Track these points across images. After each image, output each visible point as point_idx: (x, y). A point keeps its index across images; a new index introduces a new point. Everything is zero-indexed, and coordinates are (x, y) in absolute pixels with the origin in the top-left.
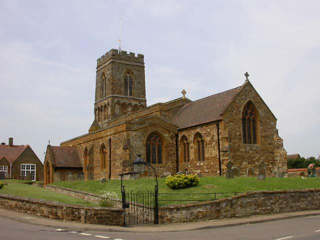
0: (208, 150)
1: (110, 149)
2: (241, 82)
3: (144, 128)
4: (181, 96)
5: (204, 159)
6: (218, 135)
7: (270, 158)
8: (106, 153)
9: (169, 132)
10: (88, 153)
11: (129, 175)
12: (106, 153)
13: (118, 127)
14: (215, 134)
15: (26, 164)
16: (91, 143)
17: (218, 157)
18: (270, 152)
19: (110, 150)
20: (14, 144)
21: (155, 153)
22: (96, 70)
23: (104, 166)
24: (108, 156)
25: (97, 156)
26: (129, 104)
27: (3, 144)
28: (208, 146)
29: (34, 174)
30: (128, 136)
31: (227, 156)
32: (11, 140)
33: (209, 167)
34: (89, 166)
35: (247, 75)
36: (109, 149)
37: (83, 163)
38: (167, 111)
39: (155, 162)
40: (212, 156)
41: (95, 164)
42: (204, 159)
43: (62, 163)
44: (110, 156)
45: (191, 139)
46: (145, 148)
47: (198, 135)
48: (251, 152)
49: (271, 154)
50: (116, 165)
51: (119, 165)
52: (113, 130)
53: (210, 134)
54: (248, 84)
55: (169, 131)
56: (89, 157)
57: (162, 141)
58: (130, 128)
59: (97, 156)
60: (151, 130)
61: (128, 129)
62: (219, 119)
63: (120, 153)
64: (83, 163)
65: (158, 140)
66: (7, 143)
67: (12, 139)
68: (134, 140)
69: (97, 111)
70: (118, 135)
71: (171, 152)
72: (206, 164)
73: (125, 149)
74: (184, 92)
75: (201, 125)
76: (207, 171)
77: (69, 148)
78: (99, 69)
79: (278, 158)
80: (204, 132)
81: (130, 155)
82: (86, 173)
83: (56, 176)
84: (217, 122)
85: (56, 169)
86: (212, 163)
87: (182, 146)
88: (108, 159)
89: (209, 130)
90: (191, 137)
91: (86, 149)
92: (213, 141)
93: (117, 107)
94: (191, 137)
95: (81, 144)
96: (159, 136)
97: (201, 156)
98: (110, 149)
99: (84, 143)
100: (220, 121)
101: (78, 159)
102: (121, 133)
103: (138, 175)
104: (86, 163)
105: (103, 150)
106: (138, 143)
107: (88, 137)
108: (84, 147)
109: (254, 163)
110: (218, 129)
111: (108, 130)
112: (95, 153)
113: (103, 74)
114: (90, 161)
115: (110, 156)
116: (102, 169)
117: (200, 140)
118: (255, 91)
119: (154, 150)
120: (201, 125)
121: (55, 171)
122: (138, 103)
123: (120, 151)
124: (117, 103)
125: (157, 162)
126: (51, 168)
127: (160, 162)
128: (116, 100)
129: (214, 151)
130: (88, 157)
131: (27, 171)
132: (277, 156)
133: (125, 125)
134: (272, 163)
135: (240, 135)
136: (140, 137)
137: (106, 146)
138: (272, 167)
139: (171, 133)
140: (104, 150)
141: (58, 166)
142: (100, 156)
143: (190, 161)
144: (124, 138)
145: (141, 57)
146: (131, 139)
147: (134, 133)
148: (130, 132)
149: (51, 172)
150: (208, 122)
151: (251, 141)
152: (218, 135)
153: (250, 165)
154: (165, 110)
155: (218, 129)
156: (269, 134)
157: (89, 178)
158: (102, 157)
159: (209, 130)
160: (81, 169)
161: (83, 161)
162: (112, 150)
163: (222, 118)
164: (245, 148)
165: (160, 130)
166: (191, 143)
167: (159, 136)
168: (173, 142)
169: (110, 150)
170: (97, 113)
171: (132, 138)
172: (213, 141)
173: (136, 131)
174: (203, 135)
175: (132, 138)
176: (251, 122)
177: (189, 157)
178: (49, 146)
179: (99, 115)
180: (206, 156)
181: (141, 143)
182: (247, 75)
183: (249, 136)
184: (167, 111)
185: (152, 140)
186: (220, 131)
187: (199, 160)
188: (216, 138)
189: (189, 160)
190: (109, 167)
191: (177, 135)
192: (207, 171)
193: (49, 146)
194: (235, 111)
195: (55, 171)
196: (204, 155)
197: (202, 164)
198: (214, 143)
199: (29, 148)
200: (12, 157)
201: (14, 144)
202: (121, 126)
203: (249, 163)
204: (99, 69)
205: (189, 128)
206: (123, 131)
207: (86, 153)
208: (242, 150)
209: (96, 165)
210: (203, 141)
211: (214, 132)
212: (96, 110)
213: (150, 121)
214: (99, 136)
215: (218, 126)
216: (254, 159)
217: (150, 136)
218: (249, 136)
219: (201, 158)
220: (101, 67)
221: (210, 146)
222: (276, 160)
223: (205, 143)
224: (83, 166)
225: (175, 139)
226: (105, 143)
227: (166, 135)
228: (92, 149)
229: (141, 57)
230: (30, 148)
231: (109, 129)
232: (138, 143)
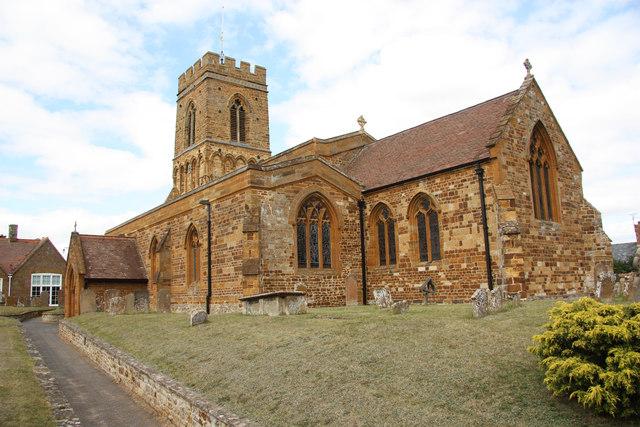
0: (451, 233)
1: (210, 235)
2: (514, 82)
3: (291, 184)
4: (357, 128)
5: (437, 256)
6: (483, 197)
7: (578, 253)
8: (199, 245)
9: (346, 196)
10: (160, 246)
11: (277, 299)
12: (199, 245)
13: (229, 182)
14: (471, 195)
15: (42, 275)
16: (165, 225)
17: (482, 249)
18: (577, 241)
19: (209, 239)
20: (20, 236)
21: (315, 243)
22: (177, 98)
23: (193, 275)
24: (203, 254)
25: (179, 253)
26: (241, 158)
27: (2, 236)
28: (450, 225)
29: (53, 298)
30: (256, 200)
31: (517, 246)
32: (14, 229)
33: (455, 273)
34: (162, 275)
35: (528, 65)
36: (206, 236)
37: (149, 269)
38: (331, 156)
39: (317, 266)
40: (464, 247)
41: (175, 271)
42: (437, 256)
43: (101, 269)
44: (210, 254)
45: (402, 209)
46: (294, 232)
47: (422, 200)
48: (548, 238)
49: (579, 245)
50: (224, 273)
51: (232, 272)
52: (218, 190)
53: (456, 197)
54: (532, 85)
55: (345, 194)
56: (161, 257)
57: (330, 218)
58: (261, 183)
59: (179, 253)
60: (307, 189)
61: (256, 185)
62: (482, 156)
63: (234, 244)
64: (149, 269)
65: (322, 215)
66: (6, 233)
67: (17, 226)
68: (268, 213)
69: (178, 174)
70: (228, 202)
71: (352, 242)
72: (445, 267)
73: (249, 233)
74: (362, 121)
75: (429, 176)
76: (448, 283)
77: (121, 241)
78: (181, 95)
79: (592, 254)
80: (440, 192)
81: (261, 247)
82: (152, 288)
83: (86, 299)
84: (478, 166)
85: (88, 283)
86: (464, 266)
87: (375, 228)
88: (204, 259)
89: (452, 187)
90: (400, 205)
91: (154, 240)
92: (467, 211)
93: (218, 160)
94: (400, 205)
95: (143, 229)
96: (324, 205)
97: (429, 245)
98: (210, 235)
99: (150, 226)
100: (487, 161)
101: (138, 261)
102: (238, 195)
103: (303, 302)
104: (153, 268)
105: (191, 239)
106: (279, 219)
107: (159, 214)
108: (151, 236)
109: (556, 265)
110: (481, 181)
111: (204, 192)
112: (174, 247)
113: (191, 104)
114: (162, 264)
115: (210, 254)
116: (190, 282)
117: (424, 212)
118: (546, 103)
119: (314, 236)
120: (429, 176)
121: (85, 288)
122: (255, 157)
123: (234, 239)
124: (216, 154)
125: (321, 264)
126: (77, 281)
127: (327, 265)
128: (215, 149)
129: (470, 237)
130: (158, 255)
131: (54, 288)
132: (590, 249)
133: (249, 173)
134: (582, 265)
135: (528, 198)
136: (283, 206)
137: (199, 229)
138: (582, 272)
139: (350, 200)
140: (195, 239)
141: (92, 276)
142: (185, 254)
143: (399, 263)
144: (247, 207)
145: (261, 71)
146: (263, 210)
147: (270, 195)
148: (259, 193)
149: (77, 289)
150: (448, 167)
151: (543, 214)
152: (483, 197)
153: (549, 268)
154: (328, 153)
155: (481, 181)
156: (572, 199)
157: (159, 305)
158: (189, 256)
159: (452, 187)
160: (145, 282)
161: (148, 265)
162: (214, 238)
163: (493, 155)
164: (538, 228)
165: (326, 190)
166: (401, 219)
167: (324, 205)
168: (354, 218)
169: (209, 239)
170: (179, 178)
171: (266, 207)
172: (467, 211)
173: (273, 189)
174: (436, 201)
175: (266, 207)
176: (542, 169)
177: (393, 251)
178: (75, 235)
179: (182, 180)
180: (446, 247)
181: (285, 221)
182: (528, 65)
183: (543, 204)
184: (331, 156)
185: (309, 215)
186: (487, 186)
187: (424, 258)
188: (475, 203)
189: (393, 261)
190: (206, 277)
191: (362, 205)
192: (448, 283)
193: (75, 235)
194: (515, 141)
195: (85, 288)
196: (437, 243)
197: (433, 268)
198: (469, 217)
199: (47, 242)
200: (16, 259)
201: (18, 237)
202: (238, 178)
203: (547, 265)
204: (181, 95)
205: (406, 181)
206: (241, 191)
207: (155, 248)
208: (534, 232)
209: (175, 274)
210: (433, 215)
211: (471, 190)
212: (175, 171)
213: (305, 169)
214: (183, 208)
215: (481, 173)
216: (555, 256)
217: (304, 205)
218: (543, 204)
219: (429, 254)
220: (186, 91)
221: (458, 224)
222: (589, 259)
223: (440, 218)
224: (149, 276)
225: (357, 212)
226: (196, 223)
227: (340, 203)
228: (166, 240)
229: (261, 71)
230: (50, 244)
231: (207, 190)
232: (279, 219)
